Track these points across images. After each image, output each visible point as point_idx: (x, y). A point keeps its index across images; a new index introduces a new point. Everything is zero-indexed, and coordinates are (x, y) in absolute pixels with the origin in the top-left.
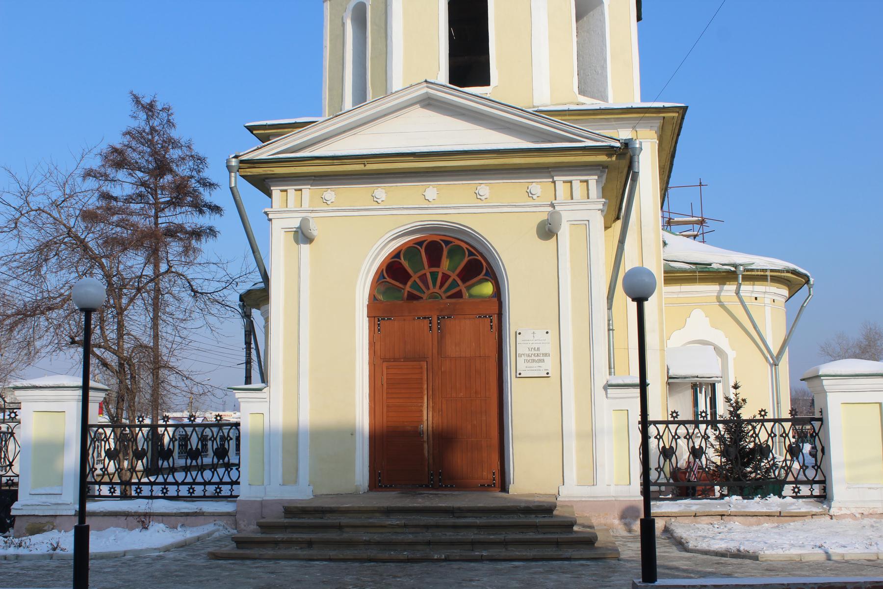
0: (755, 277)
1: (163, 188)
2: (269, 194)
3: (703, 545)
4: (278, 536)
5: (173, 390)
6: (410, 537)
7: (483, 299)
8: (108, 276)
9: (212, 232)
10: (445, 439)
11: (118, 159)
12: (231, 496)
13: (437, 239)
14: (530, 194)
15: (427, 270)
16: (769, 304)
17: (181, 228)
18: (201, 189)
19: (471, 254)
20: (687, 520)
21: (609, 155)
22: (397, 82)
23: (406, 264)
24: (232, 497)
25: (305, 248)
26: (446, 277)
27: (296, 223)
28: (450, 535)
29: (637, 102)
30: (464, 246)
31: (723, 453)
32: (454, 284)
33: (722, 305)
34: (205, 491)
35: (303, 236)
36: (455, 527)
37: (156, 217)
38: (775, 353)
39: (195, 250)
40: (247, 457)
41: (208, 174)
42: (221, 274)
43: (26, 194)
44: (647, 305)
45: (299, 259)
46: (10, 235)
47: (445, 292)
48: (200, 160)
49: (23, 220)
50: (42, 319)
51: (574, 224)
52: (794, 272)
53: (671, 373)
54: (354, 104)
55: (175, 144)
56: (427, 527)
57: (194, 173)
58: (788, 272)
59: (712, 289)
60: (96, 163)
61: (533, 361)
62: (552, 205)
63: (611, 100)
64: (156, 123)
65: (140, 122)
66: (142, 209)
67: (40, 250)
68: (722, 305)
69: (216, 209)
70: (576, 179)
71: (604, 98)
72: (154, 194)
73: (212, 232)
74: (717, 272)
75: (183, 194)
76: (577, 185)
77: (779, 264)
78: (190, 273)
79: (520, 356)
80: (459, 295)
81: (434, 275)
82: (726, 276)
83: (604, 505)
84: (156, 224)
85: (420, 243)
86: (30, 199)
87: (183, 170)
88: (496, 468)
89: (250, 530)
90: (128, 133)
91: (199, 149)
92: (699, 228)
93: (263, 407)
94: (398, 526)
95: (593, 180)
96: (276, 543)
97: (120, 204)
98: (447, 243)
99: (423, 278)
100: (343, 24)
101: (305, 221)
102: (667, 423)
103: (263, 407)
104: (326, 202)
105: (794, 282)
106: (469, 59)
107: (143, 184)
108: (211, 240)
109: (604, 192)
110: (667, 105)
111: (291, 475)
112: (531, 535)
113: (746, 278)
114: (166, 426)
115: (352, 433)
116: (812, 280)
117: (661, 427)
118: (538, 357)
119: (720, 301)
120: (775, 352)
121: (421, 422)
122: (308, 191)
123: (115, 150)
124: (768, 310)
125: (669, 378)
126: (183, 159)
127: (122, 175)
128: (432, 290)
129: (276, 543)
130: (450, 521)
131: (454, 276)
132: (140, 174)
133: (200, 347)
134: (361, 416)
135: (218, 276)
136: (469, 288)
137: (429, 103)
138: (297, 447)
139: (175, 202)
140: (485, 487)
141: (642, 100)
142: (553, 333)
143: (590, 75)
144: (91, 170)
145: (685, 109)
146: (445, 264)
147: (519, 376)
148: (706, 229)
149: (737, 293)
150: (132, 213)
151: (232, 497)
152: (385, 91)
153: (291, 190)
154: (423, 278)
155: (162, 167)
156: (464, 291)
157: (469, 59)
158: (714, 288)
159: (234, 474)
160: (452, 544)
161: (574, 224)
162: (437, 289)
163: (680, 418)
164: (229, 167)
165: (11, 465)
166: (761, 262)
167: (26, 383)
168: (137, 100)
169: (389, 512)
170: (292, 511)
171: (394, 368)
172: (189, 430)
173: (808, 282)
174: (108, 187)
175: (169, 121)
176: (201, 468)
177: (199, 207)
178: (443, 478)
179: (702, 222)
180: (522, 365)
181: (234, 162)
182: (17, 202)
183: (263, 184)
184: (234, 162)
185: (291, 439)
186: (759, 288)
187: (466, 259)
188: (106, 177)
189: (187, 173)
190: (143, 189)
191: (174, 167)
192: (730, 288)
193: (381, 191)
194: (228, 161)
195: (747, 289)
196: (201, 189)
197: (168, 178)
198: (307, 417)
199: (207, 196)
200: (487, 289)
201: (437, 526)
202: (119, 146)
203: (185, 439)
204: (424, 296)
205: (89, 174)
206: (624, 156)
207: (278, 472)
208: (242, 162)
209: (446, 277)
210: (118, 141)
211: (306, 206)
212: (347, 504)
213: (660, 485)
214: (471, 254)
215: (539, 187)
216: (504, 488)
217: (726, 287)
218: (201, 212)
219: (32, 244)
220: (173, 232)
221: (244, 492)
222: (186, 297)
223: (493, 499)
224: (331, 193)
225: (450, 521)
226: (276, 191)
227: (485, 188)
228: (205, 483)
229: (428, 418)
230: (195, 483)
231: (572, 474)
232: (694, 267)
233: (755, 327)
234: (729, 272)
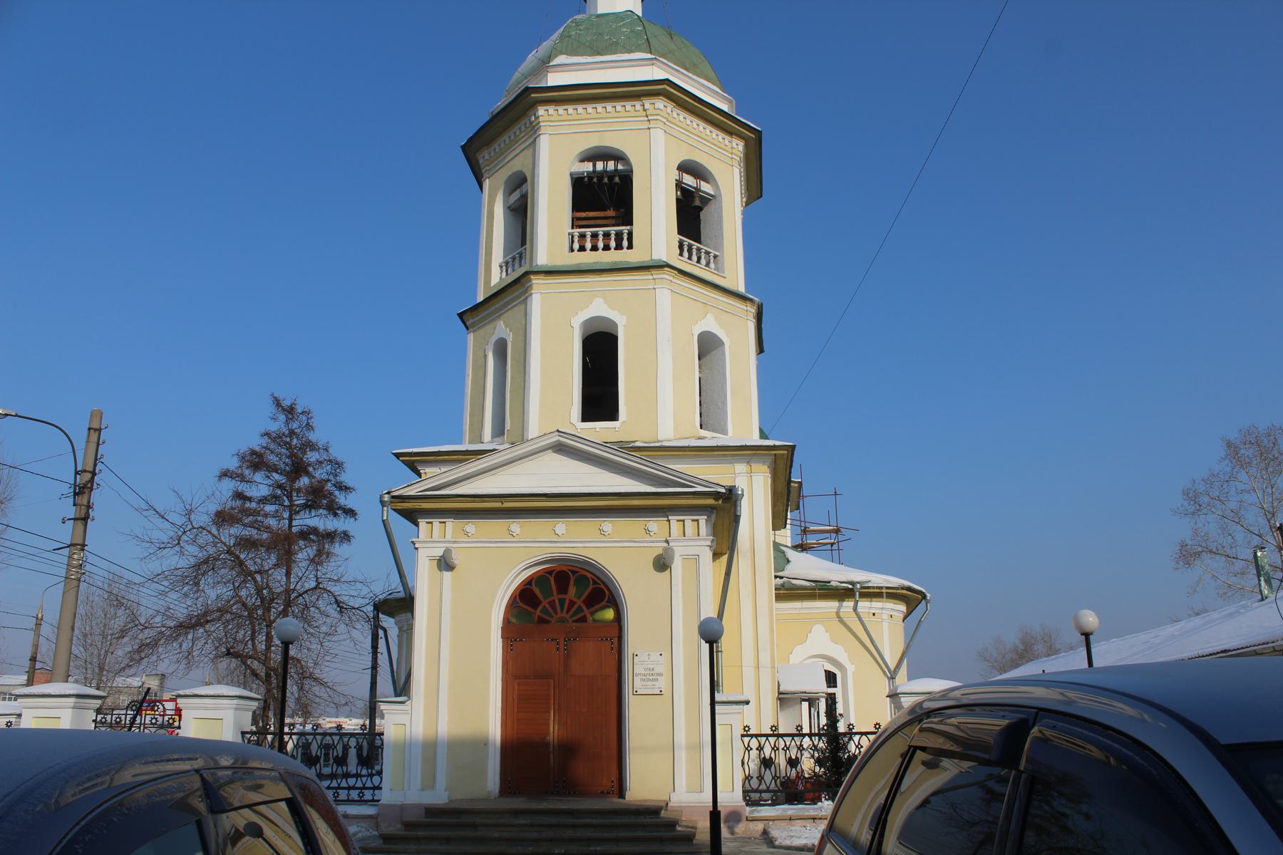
0: (872, 593)
1: (299, 490)
2: (417, 525)
3: (787, 842)
4: (420, 833)
5: (317, 700)
6: (535, 835)
7: (605, 623)
8: (259, 591)
9: (346, 537)
10: (568, 750)
11: (256, 461)
12: (373, 800)
13: (565, 569)
14: (647, 531)
15: (556, 598)
16: (886, 619)
17: (315, 530)
18: (337, 493)
19: (595, 582)
20: (783, 824)
21: (716, 499)
22: (533, 430)
23: (537, 591)
24: (374, 801)
25: (447, 574)
26: (572, 603)
27: (440, 552)
28: (569, 833)
29: (755, 440)
30: (589, 575)
31: (819, 762)
32: (579, 610)
33: (842, 621)
34: (348, 795)
35: (445, 564)
36: (574, 826)
37: (291, 520)
38: (892, 668)
39: (328, 554)
40: (389, 761)
41: (345, 478)
42: (365, 591)
43: (189, 513)
44: (725, 643)
45: (441, 584)
46: (173, 551)
47: (573, 615)
48: (337, 465)
49: (184, 537)
50: (201, 630)
51: (686, 558)
52: (909, 589)
53: (782, 689)
54: (493, 437)
55: (312, 446)
56: (550, 826)
57: (331, 477)
58: (903, 588)
59: (832, 605)
60: (233, 464)
62: (667, 542)
63: (730, 433)
64: (294, 425)
65: (278, 425)
66: (277, 511)
67: (197, 566)
68: (842, 621)
69: (350, 512)
70: (688, 519)
71: (724, 432)
72: (290, 497)
73: (346, 537)
74: (836, 589)
75: (320, 498)
76: (689, 523)
77: (894, 581)
78: (336, 589)
80: (584, 619)
81: (562, 602)
82: (844, 593)
83: (692, 808)
84: (290, 526)
85: (549, 572)
86: (193, 517)
87: (320, 474)
88: (614, 777)
89: (394, 828)
90: (267, 434)
91: (336, 453)
92: (830, 541)
93: (405, 719)
94: (526, 825)
95: (702, 519)
96: (418, 839)
97: (254, 505)
98: (574, 572)
99: (552, 604)
100: (485, 356)
101: (448, 551)
102: (792, 736)
103: (405, 719)
104: (467, 534)
105: (911, 599)
106: (600, 397)
107: (280, 486)
108: (345, 546)
109: (715, 531)
110: (778, 443)
111: (429, 782)
112: (640, 833)
113: (863, 595)
114: (291, 734)
115: (485, 743)
116: (928, 596)
117: (788, 739)
118: (652, 676)
119: (839, 617)
120: (892, 667)
121: (548, 734)
122: (450, 523)
123: (253, 453)
124: (885, 625)
125: (780, 693)
126: (321, 463)
127: (259, 477)
128: (560, 614)
129: (418, 839)
130: (570, 821)
131: (579, 602)
132: (276, 476)
133: (340, 658)
134: (493, 728)
135: (363, 593)
136: (593, 613)
137: (560, 448)
138: (435, 752)
139: (309, 506)
140: (604, 794)
141: (763, 435)
142: (667, 654)
143: (710, 414)
144: (228, 471)
145: (793, 447)
146: (572, 590)
147: (635, 694)
148: (841, 538)
149: (855, 609)
150: (266, 516)
151: (374, 801)
152: (523, 440)
153: (436, 522)
154: (552, 604)
155: (299, 468)
156: (588, 615)
157: (600, 397)
158: (835, 604)
159: (376, 779)
160: (571, 840)
161: (686, 558)
162: (565, 617)
163: (751, 732)
164: (383, 503)
166: (878, 580)
167: (188, 692)
168: (277, 403)
169: (517, 813)
170: (431, 811)
171: (526, 683)
172: (310, 738)
173: (924, 597)
174: (242, 487)
175: (308, 424)
176: (347, 775)
177: (333, 509)
178: (567, 786)
179: (837, 531)
181: (386, 498)
182: (180, 520)
183: (412, 516)
184: (386, 498)
185: (430, 748)
186: (876, 604)
187: (591, 587)
188: (242, 478)
189: (325, 477)
190: (279, 492)
191: (311, 469)
192: (848, 604)
193: (516, 526)
194: (381, 497)
195: (864, 605)
196: (337, 493)
197: (304, 481)
198: (445, 728)
199: (341, 499)
200: (609, 614)
201: (559, 826)
202: (257, 449)
203: (307, 746)
204: (553, 620)
205: (225, 474)
206: (722, 507)
207: (417, 782)
208: (393, 497)
209: (572, 603)
210: (256, 443)
211: (449, 537)
212: (480, 806)
213: (761, 792)
214: (595, 582)
215: (655, 525)
216: (621, 794)
217: (845, 604)
218: (335, 515)
219: (193, 561)
220: (306, 534)
221: (388, 795)
222: (332, 611)
223: (614, 802)
224: (471, 526)
225: (570, 821)
226: (422, 523)
227: (608, 524)
228: (349, 788)
229: (554, 731)
230: (339, 788)
231: (681, 782)
232: (808, 584)
233: (873, 642)
234: (847, 589)
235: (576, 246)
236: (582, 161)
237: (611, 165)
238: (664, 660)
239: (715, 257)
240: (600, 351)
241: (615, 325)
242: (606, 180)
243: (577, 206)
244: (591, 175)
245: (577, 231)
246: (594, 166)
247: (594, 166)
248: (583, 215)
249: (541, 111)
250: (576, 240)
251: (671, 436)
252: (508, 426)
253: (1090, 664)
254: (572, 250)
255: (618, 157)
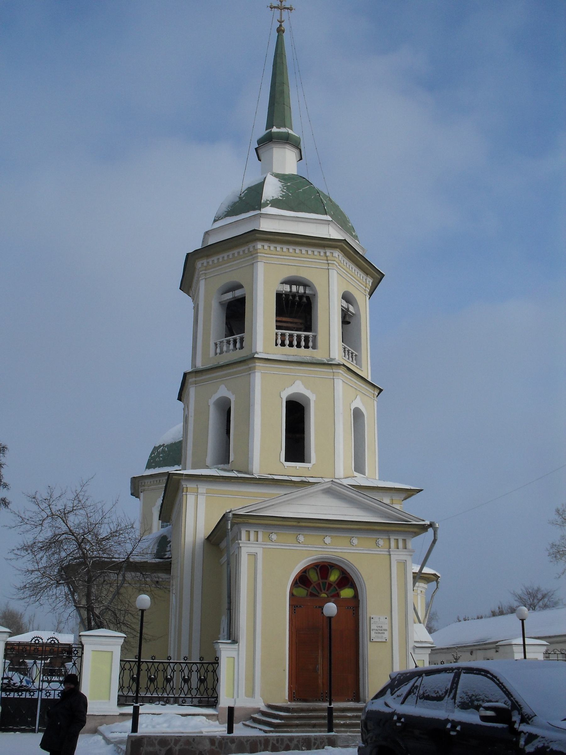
61: (379, 633)
63: (366, 475)
79: (373, 630)
118: (381, 631)
131: (321, 581)
142: (389, 618)
161: (250, 554)
165: (33, 682)
180: (373, 634)
235: (279, 341)
236: (282, 283)
237: (301, 290)
238: (387, 621)
239: (356, 355)
240: (296, 412)
241: (308, 400)
242: (297, 298)
243: (280, 312)
244: (287, 295)
245: (280, 332)
246: (291, 288)
247: (291, 288)
248: (284, 319)
249: (259, 245)
250: (279, 337)
251: (342, 476)
252: (232, 458)
253: (525, 657)
254: (276, 345)
255: (306, 285)
